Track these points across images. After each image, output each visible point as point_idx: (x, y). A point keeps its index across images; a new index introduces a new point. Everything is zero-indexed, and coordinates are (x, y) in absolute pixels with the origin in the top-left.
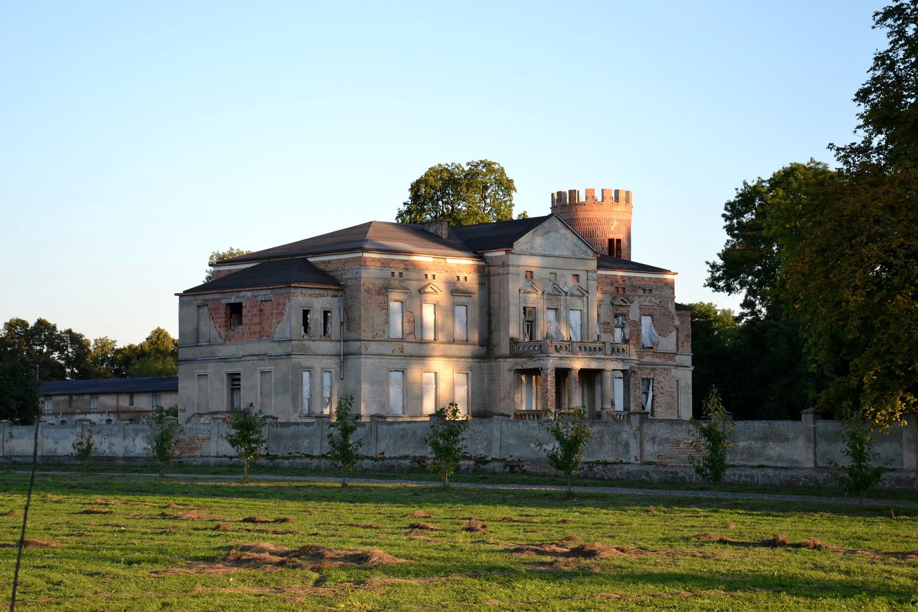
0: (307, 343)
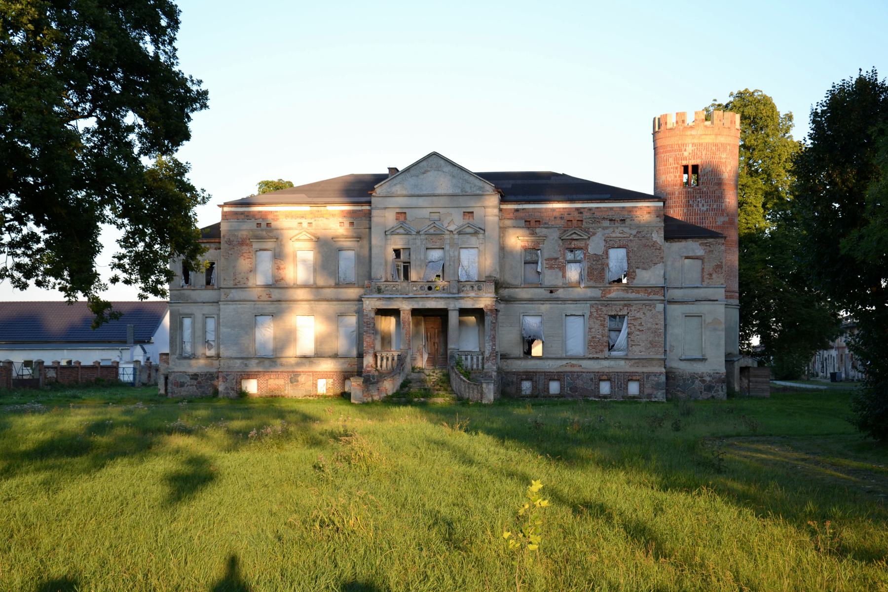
0: (187, 292)
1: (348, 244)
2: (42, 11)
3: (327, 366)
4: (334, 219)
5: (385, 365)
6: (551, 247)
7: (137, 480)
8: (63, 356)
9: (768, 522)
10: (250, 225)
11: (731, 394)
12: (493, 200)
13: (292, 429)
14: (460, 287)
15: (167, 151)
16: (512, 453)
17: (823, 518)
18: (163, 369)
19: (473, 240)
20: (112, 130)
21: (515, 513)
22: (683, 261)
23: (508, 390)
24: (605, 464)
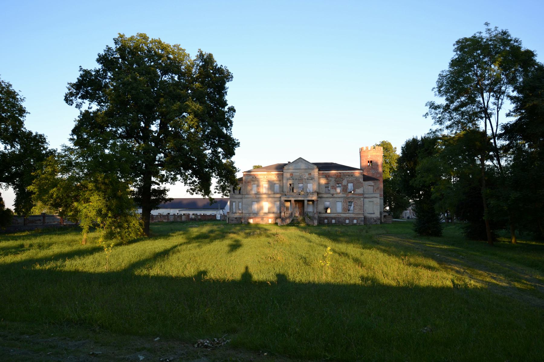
1: (277, 182)
2: (198, 123)
3: (271, 215)
4: (273, 176)
5: (287, 215)
6: (332, 183)
7: (220, 246)
8: (202, 213)
9: (391, 257)
10: (251, 177)
11: (381, 223)
12: (316, 170)
13: (262, 232)
14: (307, 194)
15: (229, 158)
16: (322, 239)
17: (405, 255)
18: (228, 216)
19: (311, 181)
20: (215, 153)
21: (323, 256)
22: (368, 186)
23: (321, 222)
24: (348, 242)
